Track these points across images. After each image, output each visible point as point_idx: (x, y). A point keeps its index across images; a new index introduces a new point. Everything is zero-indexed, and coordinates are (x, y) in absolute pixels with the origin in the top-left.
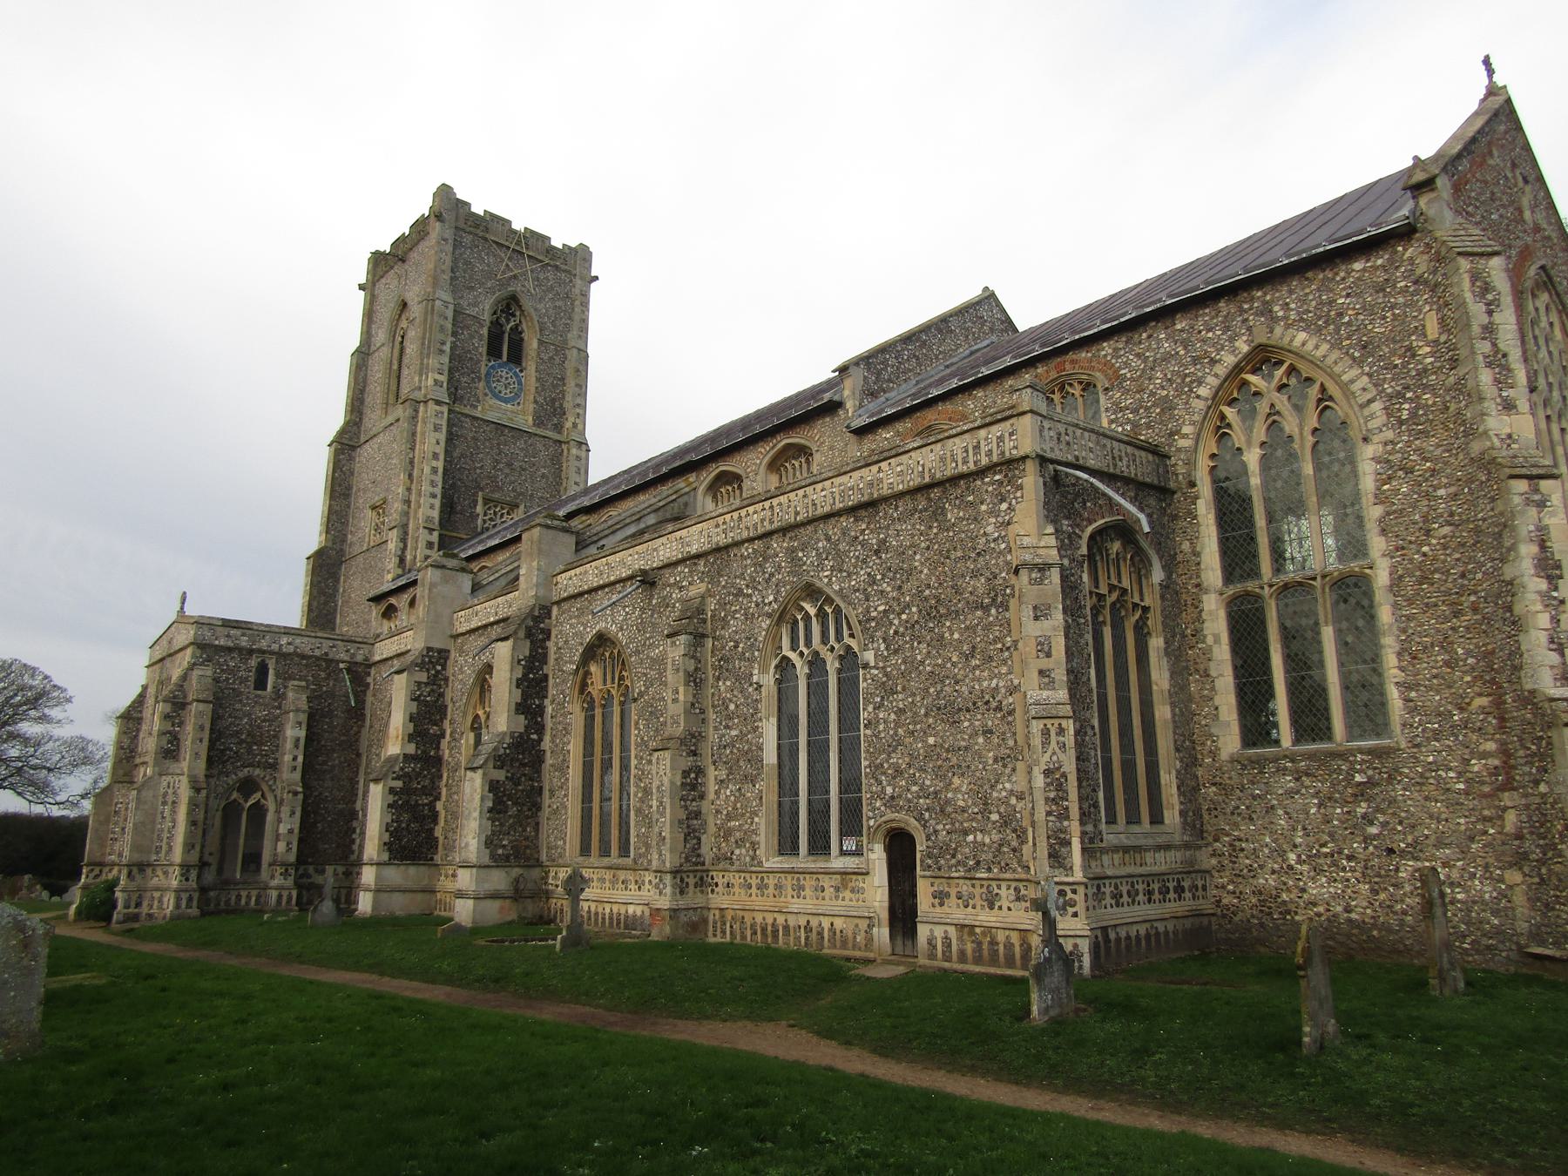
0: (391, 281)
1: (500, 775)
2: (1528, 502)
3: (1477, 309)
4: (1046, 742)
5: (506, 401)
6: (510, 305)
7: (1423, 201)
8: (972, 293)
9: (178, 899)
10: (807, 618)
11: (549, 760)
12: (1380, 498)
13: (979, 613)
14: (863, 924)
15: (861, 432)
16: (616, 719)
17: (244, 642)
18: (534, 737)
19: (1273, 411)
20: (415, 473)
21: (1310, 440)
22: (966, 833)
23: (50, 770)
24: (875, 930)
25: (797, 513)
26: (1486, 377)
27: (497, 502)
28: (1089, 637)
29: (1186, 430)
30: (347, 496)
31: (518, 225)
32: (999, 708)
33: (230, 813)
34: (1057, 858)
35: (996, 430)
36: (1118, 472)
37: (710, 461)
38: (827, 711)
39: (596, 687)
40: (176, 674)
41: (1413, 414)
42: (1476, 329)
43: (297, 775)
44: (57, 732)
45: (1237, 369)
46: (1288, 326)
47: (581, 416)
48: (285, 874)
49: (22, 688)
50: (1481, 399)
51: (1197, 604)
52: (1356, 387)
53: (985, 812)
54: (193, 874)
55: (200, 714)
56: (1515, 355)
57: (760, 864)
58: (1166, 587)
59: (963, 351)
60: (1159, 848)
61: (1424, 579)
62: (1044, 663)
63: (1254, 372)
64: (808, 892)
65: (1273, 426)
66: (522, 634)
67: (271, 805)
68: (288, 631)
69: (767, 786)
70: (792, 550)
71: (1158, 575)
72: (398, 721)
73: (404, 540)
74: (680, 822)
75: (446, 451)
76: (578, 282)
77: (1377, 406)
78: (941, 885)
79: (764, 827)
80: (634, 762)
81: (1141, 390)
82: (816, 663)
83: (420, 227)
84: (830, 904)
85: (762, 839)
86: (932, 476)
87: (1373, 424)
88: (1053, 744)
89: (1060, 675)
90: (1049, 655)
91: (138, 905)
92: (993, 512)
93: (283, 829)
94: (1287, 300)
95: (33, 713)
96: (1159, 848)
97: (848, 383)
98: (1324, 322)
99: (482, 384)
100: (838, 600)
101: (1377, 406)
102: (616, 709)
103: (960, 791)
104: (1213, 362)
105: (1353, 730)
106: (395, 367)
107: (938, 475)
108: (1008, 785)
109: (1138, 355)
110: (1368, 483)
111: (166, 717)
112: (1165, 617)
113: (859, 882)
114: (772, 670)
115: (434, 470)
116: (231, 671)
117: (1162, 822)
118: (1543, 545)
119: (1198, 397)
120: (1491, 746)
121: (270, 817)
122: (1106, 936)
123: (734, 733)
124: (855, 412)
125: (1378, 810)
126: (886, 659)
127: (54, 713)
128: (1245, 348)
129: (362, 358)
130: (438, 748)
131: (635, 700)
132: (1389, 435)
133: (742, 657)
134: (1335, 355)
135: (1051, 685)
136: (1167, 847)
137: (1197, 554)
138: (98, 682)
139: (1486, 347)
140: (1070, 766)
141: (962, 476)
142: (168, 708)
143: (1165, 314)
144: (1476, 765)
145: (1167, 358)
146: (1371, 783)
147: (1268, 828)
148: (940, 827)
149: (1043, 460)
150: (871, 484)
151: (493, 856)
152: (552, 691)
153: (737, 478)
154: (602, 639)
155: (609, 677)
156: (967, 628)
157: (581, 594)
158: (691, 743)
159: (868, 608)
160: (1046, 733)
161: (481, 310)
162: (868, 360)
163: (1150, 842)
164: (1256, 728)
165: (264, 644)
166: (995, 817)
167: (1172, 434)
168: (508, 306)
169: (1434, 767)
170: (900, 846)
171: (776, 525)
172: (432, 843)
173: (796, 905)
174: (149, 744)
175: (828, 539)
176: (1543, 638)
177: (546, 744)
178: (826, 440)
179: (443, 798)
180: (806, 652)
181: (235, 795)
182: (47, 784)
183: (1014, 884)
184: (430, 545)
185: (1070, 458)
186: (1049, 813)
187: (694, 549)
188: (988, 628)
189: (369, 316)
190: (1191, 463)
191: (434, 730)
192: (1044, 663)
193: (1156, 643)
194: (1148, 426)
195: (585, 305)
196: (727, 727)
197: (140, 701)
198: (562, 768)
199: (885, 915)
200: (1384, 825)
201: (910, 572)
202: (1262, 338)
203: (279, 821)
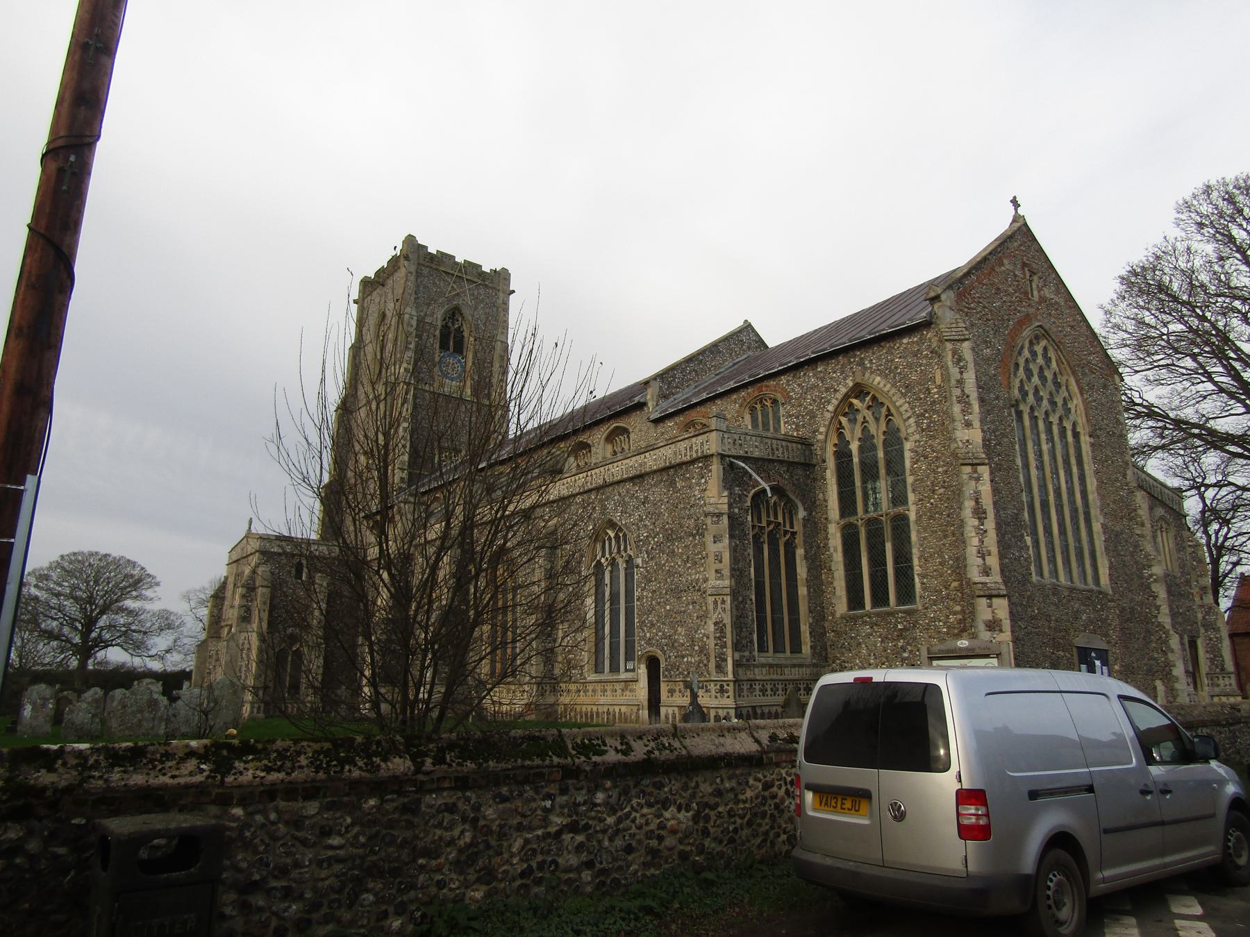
2: (971, 478)
3: (954, 371)
4: (715, 608)
6: (454, 313)
7: (936, 306)
8: (734, 324)
9: (252, 708)
10: (610, 539)
12: (913, 472)
14: (635, 709)
15: (657, 421)
19: (865, 421)
21: (882, 437)
22: (683, 657)
23: (145, 633)
26: (957, 409)
28: (751, 551)
29: (822, 429)
31: (459, 259)
33: (280, 658)
34: (720, 668)
40: (247, 571)
41: (928, 426)
42: (953, 382)
44: (148, 606)
45: (847, 396)
46: (872, 373)
48: (315, 693)
49: (126, 576)
50: (954, 421)
51: (826, 529)
52: (902, 409)
53: (692, 645)
55: (263, 595)
56: (974, 397)
58: (806, 521)
59: (728, 364)
60: (794, 666)
61: (931, 517)
62: (718, 566)
64: (609, 693)
70: (601, 501)
71: (802, 514)
76: (501, 295)
77: (912, 420)
78: (671, 685)
79: (585, 656)
81: (800, 405)
83: (394, 261)
84: (620, 699)
87: (910, 431)
89: (726, 572)
92: (698, 484)
94: (872, 358)
95: (134, 593)
96: (794, 666)
97: (649, 391)
98: (888, 372)
101: (912, 420)
103: (681, 635)
104: (836, 391)
110: (908, 464)
111: (243, 596)
113: (632, 686)
117: (800, 652)
118: (977, 501)
120: (958, 608)
124: (653, 411)
125: (908, 644)
127: (149, 593)
128: (851, 384)
132: (917, 437)
134: (893, 391)
135: (721, 578)
136: (800, 666)
137: (826, 501)
139: (957, 392)
140: (727, 620)
142: (244, 591)
143: (811, 362)
144: (952, 618)
145: (814, 387)
146: (905, 629)
147: (858, 655)
149: (722, 457)
160: (715, 602)
161: (435, 316)
163: (789, 662)
164: (855, 600)
168: (454, 314)
169: (934, 619)
170: (653, 664)
173: (603, 700)
174: (231, 613)
176: (974, 550)
178: (637, 425)
182: (143, 643)
184: (402, 479)
185: (742, 453)
189: (361, 323)
190: (824, 449)
192: (718, 566)
193: (800, 552)
199: (646, 704)
200: (911, 652)
202: (858, 380)
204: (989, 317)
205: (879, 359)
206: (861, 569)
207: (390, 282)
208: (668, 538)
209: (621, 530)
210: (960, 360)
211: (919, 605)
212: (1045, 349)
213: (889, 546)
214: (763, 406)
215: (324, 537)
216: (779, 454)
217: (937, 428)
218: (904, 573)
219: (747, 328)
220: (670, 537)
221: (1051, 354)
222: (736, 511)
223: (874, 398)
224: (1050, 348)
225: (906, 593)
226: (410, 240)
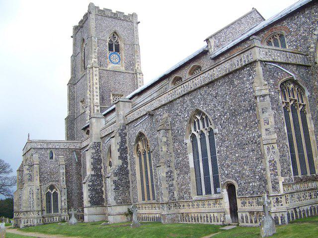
0: (79, 33)
1: (116, 178)
11: (130, 173)
13: (247, 113)
14: (222, 214)
16: (148, 158)
18: (125, 166)
20: (92, 89)
22: (249, 183)
24: (226, 215)
25: (191, 88)
29: (312, 46)
30: (74, 99)
32: (256, 143)
36: (289, 62)
37: (173, 76)
38: (207, 150)
39: (141, 148)
43: (65, 183)
53: (254, 176)
54: (40, 213)
57: (192, 199)
64: (206, 206)
66: (118, 135)
67: (59, 192)
68: (59, 142)
69: (192, 175)
71: (307, 94)
72: (116, 154)
73: (90, 110)
74: (167, 188)
75: (99, 81)
80: (153, 171)
82: (202, 134)
85: (191, 191)
86: (229, 71)
88: (271, 152)
90: (268, 124)
91: (27, 222)
92: (248, 80)
93: (63, 199)
99: (108, 60)
100: (206, 114)
102: (147, 155)
106: (83, 59)
107: (231, 70)
108: (260, 167)
109: (294, 24)
112: (311, 107)
114: (190, 138)
115: (96, 88)
119: (315, 35)
121: (59, 196)
122: (296, 212)
123: (180, 159)
126: (221, 131)
129: (74, 57)
130: (101, 171)
131: (152, 152)
133: (180, 135)
138: (15, 160)
140: (277, 159)
141: (237, 70)
148: (242, 182)
150: (211, 76)
153: (180, 78)
154: (141, 134)
155: (144, 147)
156: (244, 118)
157: (134, 121)
159: (215, 115)
160: (268, 149)
166: (257, 177)
167: (308, 48)
170: (231, 188)
171: (186, 92)
172: (102, 200)
175: (201, 95)
177: (129, 168)
178: (205, 63)
179: (104, 187)
180: (199, 131)
181: (49, 190)
183: (275, 197)
186: (271, 174)
187: (163, 103)
188: (250, 117)
189: (75, 45)
191: (99, 167)
192: (267, 127)
193: (309, 116)
194: (300, 46)
196: (178, 157)
198: (134, 175)
199: (228, 211)
201: (226, 102)
209: (204, 114)
219: (255, 11)
220: (234, 114)
222: (273, 93)
226: (91, 6)
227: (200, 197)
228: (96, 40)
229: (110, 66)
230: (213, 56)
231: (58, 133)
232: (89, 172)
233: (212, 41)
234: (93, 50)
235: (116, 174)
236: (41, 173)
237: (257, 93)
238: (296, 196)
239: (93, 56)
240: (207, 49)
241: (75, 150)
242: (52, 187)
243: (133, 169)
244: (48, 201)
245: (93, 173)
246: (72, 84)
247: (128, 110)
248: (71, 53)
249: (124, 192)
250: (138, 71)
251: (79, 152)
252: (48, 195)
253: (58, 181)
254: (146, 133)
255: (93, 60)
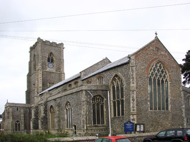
1: (42, 120)
4: (82, 118)
5: (51, 68)
11: (48, 119)
17: (15, 105)
20: (38, 80)
27: (51, 83)
35: (81, 87)
39: (52, 111)
40: (8, 109)
43: (23, 120)
47: (63, 69)
54: (12, 131)
63: (116, 77)
65: (117, 83)
67: (21, 123)
72: (42, 112)
73: (37, 89)
75: (42, 77)
76: (62, 49)
79: (65, 125)
93: (22, 126)
94: (119, 69)
99: (47, 66)
105: (118, 116)
115: (41, 80)
116: (14, 109)
121: (21, 125)
129: (30, 63)
146: (122, 120)
147: (115, 124)
151: (42, 128)
152: (48, 111)
158: (59, 117)
160: (82, 117)
161: (46, 56)
162: (84, 71)
165: (17, 106)
170: (75, 126)
176: (132, 106)
177: (48, 117)
184: (41, 90)
185: (90, 89)
187: (59, 97)
189: (31, 56)
191: (37, 115)
195: (63, 52)
197: (4, 112)
198: (49, 119)
203: (22, 125)
204: (144, 60)
205: (120, 69)
206: (120, 108)
207: (36, 48)
208: (77, 105)
210: (133, 70)
211: (124, 116)
212: (160, 65)
213: (120, 105)
214: (101, 78)
215: (27, 103)
216: (99, 89)
217: (129, 84)
218: (123, 110)
219: (107, 59)
221: (162, 66)
223: (119, 77)
224: (161, 65)
225: (123, 114)
226: (39, 39)
227: (67, 129)
228: (41, 57)
229: (48, 70)
230: (81, 79)
231: (22, 100)
232: (33, 117)
233: (82, 74)
234: (39, 62)
235: (42, 119)
236: (13, 116)
237: (82, 100)
238: (93, 130)
239: (39, 64)
240: (80, 76)
241: (28, 108)
242: (18, 121)
243: (49, 118)
244: (16, 126)
245: (35, 117)
246: (29, 76)
247: (48, 96)
248: (29, 60)
249: (45, 125)
250: (62, 72)
251: (30, 109)
252: (16, 124)
253: (20, 119)
254: (53, 106)
255: (39, 66)
